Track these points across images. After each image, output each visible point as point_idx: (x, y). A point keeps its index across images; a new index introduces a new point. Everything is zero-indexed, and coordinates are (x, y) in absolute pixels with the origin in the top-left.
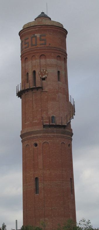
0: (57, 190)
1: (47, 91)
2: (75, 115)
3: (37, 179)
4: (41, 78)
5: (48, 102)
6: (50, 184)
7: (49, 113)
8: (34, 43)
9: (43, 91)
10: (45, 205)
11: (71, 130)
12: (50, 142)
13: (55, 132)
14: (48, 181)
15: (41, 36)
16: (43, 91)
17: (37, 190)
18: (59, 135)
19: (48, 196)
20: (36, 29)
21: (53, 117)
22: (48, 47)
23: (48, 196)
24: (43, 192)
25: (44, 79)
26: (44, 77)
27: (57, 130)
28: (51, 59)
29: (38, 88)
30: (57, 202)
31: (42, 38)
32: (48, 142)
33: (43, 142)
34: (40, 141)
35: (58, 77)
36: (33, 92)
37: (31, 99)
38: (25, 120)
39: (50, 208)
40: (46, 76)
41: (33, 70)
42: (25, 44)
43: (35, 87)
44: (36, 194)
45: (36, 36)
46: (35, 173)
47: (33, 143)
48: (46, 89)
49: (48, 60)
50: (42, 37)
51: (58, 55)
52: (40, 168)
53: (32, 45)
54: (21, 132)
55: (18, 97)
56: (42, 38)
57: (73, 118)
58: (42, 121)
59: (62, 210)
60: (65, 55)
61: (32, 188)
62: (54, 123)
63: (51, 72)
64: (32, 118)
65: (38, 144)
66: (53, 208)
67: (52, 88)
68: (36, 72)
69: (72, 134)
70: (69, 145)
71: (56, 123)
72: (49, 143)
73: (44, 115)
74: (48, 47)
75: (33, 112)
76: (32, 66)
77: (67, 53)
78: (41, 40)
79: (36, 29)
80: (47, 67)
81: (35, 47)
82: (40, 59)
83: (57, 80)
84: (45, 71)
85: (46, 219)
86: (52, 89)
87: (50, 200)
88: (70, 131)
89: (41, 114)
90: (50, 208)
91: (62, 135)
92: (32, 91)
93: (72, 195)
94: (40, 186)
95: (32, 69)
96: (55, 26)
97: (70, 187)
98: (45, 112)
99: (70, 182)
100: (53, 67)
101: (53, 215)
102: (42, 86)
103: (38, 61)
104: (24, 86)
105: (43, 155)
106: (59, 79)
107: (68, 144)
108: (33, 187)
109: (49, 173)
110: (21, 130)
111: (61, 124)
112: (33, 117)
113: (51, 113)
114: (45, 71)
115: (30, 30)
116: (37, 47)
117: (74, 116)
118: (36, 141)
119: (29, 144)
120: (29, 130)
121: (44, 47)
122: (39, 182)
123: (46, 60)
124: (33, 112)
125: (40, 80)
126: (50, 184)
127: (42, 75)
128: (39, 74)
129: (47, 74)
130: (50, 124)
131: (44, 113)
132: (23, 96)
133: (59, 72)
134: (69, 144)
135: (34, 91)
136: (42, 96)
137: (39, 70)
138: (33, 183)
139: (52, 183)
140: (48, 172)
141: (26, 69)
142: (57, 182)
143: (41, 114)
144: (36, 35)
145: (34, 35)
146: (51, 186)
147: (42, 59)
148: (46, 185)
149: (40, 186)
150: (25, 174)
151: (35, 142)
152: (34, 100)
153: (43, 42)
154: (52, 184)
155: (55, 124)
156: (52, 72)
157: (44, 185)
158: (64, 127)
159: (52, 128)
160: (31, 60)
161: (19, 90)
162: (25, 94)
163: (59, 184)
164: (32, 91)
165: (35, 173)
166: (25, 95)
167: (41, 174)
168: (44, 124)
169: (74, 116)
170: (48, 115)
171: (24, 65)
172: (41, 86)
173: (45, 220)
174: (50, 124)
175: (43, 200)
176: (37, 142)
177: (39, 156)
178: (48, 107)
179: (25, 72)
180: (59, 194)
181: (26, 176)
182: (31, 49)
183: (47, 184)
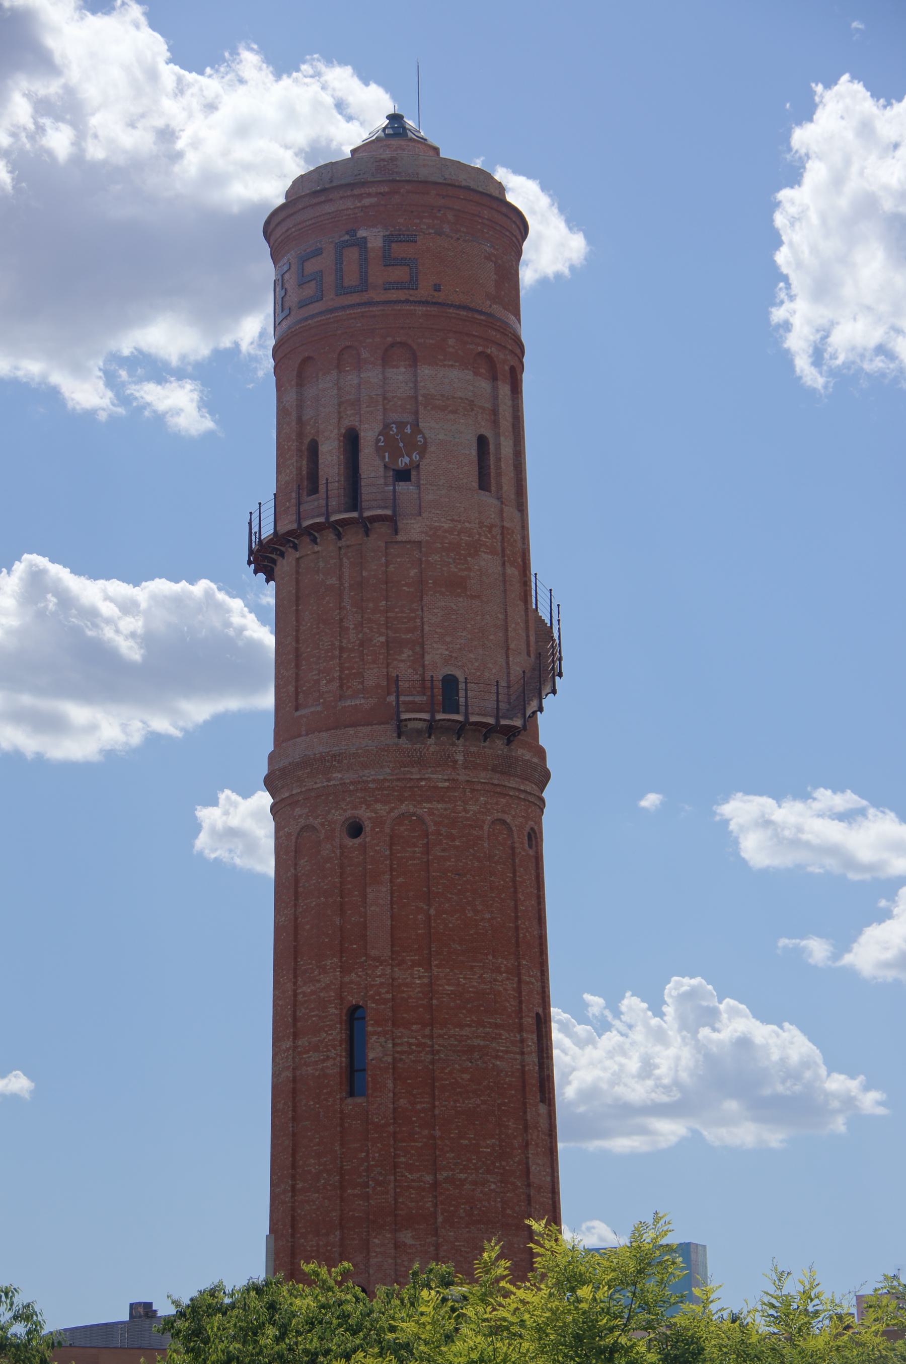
0: (466, 1076)
1: (420, 542)
2: (560, 675)
3: (354, 1016)
4: (385, 466)
5: (425, 598)
6: (429, 1042)
7: (427, 657)
8: (351, 278)
9: (399, 538)
10: (403, 1159)
11: (541, 753)
12: (431, 812)
13: (460, 758)
14: (415, 1027)
15: (389, 240)
16: (399, 538)
17: (353, 1076)
18: (483, 776)
19: (419, 1107)
20: (367, 201)
21: (450, 682)
22: (426, 303)
23: (419, 1107)
24: (390, 1085)
25: (403, 475)
26: (403, 462)
27: (473, 749)
28: (445, 366)
29: (366, 525)
30: (466, 1142)
31: (398, 250)
32: (419, 811)
33: (395, 813)
34: (378, 806)
35: (475, 468)
36: (342, 543)
37: (333, 581)
38: (297, 693)
39: (429, 1178)
40: (415, 456)
41: (346, 423)
42: (300, 285)
43: (355, 515)
44: (352, 1094)
45: (365, 238)
46: (347, 979)
47: (339, 816)
48: (413, 529)
49: (425, 371)
50: (393, 245)
51: (480, 349)
52: (373, 953)
53: (342, 290)
54: (271, 757)
55: (256, 572)
56: (398, 250)
57: (554, 692)
58: (392, 698)
59: (493, 1186)
60: (518, 351)
61: (328, 1064)
62: (458, 713)
63: (441, 437)
64: (336, 684)
65: (368, 826)
66: (445, 1174)
67: (446, 526)
68: (362, 434)
69: (546, 776)
70: (529, 835)
71: (466, 715)
72: (428, 819)
73: (404, 670)
74: (426, 303)
75: (342, 649)
76: (340, 404)
77: (524, 339)
78: (389, 260)
79: (367, 201)
80: (421, 408)
81: (354, 299)
82: (383, 366)
83: (475, 485)
84: (408, 430)
85: (407, 1237)
86: (445, 531)
87: (426, 1132)
88: (535, 760)
89: (388, 665)
90: (429, 1178)
91: (496, 779)
92: (339, 536)
93: (543, 1109)
94: (376, 1050)
95: (340, 419)
96: (468, 188)
97: (536, 1060)
98: (407, 653)
99: (535, 1037)
100: (455, 412)
101: (440, 1219)
102: (394, 511)
103: (372, 375)
104: (293, 510)
105: (391, 882)
106: (484, 483)
107: (527, 829)
108: (334, 1061)
109: (426, 981)
110: (271, 748)
111: (491, 721)
112: (340, 678)
113: (438, 661)
114: (408, 430)
115: (328, 208)
116: (370, 303)
117: (557, 678)
118: (355, 808)
119: (317, 822)
120: (318, 744)
121: (407, 301)
122: (370, 1029)
123: (415, 375)
124: (342, 649)
125: (382, 481)
126: (429, 1042)
127: (396, 454)
128: (378, 449)
129: (423, 450)
130: (498, 721)
131: (404, 656)
132: (284, 566)
133: (482, 441)
134: (532, 829)
135: (352, 538)
136: (391, 568)
137: (378, 427)
138: (337, 1034)
139: (440, 1036)
140: (420, 978)
141: (305, 418)
142: (466, 1031)
143: (388, 665)
144: (362, 233)
145: (352, 232)
146: (433, 1053)
147: (397, 367)
148: (405, 1048)
149: (371, 1055)
150: (289, 986)
151: (349, 813)
152: (347, 585)
153: (399, 273)
154: (441, 1041)
155: (459, 718)
156: (449, 439)
157: (394, 1045)
158: (510, 734)
159: (16, 588)
160: (335, 372)
161: (268, 531)
162: (298, 555)
163: (477, 1042)
164: (339, 536)
165: (347, 979)
166: (298, 559)
167: (382, 984)
168: (404, 716)
169: (557, 678)
170: (423, 666)
171: (291, 397)
172: (389, 512)
173: (397, 1246)
174: (498, 721)
175: (391, 1129)
176: (364, 814)
177: (369, 890)
178: (426, 628)
179: (300, 435)
180: (478, 1101)
181: (295, 995)
182: (335, 310)
183: (410, 1044)
